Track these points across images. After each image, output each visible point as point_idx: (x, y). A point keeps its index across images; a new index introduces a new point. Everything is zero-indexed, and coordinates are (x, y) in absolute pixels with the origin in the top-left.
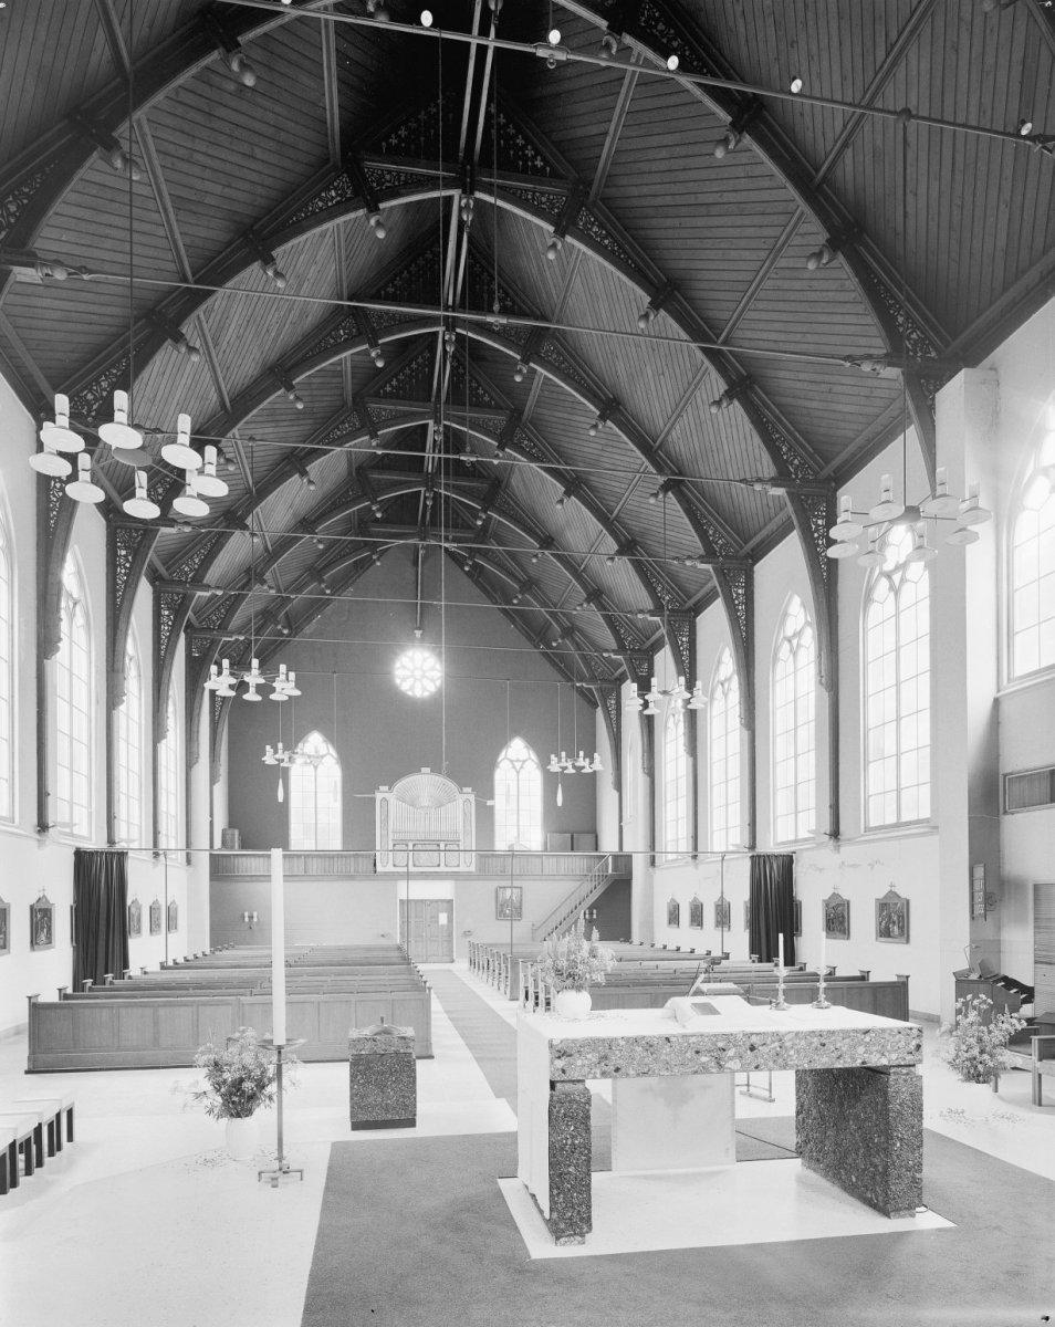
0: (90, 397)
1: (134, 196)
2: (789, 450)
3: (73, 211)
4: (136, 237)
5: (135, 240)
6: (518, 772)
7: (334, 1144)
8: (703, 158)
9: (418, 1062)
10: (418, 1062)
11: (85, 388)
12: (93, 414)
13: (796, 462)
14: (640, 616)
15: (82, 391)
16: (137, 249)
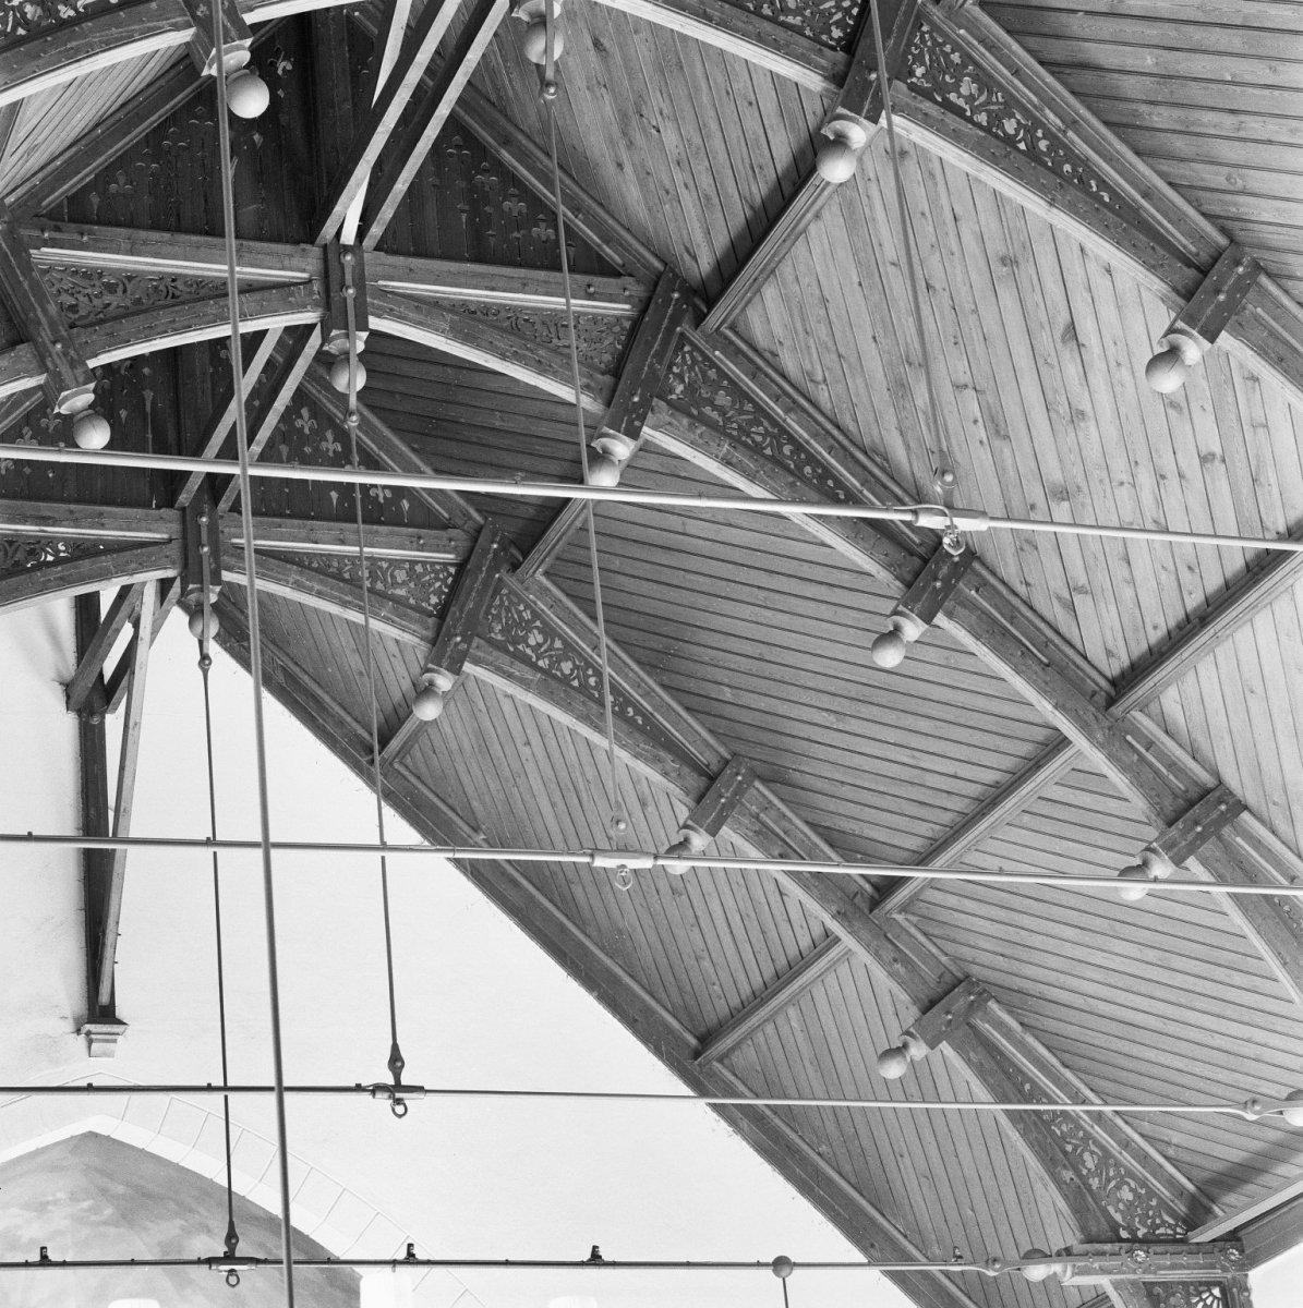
14: (1037, 1272)
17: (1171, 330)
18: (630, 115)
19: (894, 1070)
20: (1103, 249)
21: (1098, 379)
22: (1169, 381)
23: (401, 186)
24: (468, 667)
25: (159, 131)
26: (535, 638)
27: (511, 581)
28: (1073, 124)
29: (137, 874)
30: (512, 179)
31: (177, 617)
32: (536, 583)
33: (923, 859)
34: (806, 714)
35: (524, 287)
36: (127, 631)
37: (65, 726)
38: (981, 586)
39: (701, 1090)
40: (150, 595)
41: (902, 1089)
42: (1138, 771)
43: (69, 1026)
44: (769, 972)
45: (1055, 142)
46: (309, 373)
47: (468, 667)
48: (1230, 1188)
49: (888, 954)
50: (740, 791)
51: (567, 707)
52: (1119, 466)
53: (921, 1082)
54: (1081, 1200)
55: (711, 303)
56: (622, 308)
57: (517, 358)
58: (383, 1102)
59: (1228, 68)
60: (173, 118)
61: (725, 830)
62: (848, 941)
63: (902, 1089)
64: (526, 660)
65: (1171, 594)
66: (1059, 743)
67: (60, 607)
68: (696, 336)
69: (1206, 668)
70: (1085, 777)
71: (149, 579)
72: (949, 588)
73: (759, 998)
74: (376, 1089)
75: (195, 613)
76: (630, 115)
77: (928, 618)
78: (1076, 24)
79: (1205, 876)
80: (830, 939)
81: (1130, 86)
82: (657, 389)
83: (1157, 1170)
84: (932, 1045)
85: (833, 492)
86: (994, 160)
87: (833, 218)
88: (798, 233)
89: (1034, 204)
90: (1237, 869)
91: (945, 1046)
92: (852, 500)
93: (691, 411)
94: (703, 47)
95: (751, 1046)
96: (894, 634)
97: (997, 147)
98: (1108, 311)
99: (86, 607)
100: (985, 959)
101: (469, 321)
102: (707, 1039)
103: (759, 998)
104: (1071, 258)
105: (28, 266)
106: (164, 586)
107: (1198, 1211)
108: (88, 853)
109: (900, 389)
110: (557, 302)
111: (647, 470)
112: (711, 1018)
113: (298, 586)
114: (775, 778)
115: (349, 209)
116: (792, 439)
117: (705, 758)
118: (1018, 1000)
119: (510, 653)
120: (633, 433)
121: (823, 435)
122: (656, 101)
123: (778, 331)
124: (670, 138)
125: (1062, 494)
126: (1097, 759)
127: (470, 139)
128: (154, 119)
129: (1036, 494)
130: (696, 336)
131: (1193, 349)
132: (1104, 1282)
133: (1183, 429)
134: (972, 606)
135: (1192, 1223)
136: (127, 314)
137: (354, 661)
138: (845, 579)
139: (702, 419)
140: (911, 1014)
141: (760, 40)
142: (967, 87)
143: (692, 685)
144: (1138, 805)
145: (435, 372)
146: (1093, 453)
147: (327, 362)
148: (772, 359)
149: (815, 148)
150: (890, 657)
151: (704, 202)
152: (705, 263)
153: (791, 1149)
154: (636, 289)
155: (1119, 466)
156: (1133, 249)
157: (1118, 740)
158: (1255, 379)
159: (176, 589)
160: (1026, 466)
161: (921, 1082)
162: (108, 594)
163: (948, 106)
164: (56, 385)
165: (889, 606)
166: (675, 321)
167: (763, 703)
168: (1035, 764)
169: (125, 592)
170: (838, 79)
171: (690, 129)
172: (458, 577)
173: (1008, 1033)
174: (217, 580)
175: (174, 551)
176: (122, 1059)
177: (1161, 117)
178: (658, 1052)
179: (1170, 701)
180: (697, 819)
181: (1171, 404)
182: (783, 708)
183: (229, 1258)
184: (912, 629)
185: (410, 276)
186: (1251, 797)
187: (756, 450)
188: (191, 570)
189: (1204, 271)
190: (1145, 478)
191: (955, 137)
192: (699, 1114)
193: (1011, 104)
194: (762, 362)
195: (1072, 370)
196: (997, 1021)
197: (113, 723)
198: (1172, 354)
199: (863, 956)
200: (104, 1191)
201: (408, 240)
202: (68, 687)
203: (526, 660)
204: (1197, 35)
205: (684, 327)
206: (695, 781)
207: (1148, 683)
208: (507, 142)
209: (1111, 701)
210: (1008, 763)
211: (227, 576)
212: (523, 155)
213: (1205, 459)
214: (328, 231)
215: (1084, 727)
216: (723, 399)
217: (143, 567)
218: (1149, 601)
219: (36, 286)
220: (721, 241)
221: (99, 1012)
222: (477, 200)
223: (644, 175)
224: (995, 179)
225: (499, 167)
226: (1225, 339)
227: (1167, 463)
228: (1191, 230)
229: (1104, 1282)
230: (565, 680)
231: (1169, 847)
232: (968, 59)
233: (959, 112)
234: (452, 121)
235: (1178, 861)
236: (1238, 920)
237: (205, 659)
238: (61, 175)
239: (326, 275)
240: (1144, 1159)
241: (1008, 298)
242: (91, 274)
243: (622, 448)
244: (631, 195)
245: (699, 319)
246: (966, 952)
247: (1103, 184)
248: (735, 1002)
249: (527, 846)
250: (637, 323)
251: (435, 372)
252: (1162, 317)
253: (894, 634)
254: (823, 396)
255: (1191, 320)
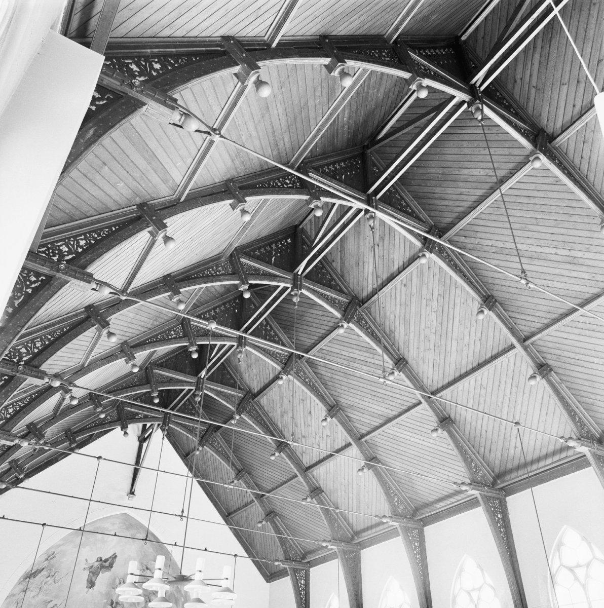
0: (65, 249)
1: (492, 156)
2: (398, 500)
3: (321, 327)
4: (382, 364)
5: (489, 157)
6: (584, 586)
7: (267, 581)
8: (580, 343)
9: (109, 138)
10: (109, 138)
11: (63, 240)
12: (22, 363)
13: (293, 552)
14: (277, 563)
15: (58, 241)
16: (495, 158)
17: (326, 416)
18: (249, 367)
19: (260, 525)
20: (317, 401)
21: (313, 419)
22: (324, 424)
23: (212, 371)
24: (205, 447)
25: (177, 355)
26: (216, 444)
27: (214, 434)
28: (316, 382)
29: (142, 473)
30: (229, 372)
31: (159, 430)
32: (218, 436)
33: (269, 492)
34: (256, 464)
35: (227, 389)
36: (151, 430)
37: (137, 443)
38: (289, 449)
39: (227, 524)
40: (156, 426)
41: (260, 529)
42: (308, 483)
43: (126, 494)
44: (242, 505)
45: (313, 384)
46: (190, 396)
47: (205, 447)
48: (310, 554)
49: (262, 505)
50: (244, 475)
51: (219, 456)
52: (314, 434)
53: (263, 529)
54: (285, 552)
55: (256, 397)
56: (242, 395)
57: (224, 400)
58: (179, 518)
59: (341, 378)
60: (180, 353)
61: (240, 481)
62: (256, 502)
63: (260, 529)
64: (214, 447)
65: (318, 456)
66: (296, 476)
67: (140, 425)
68: (252, 402)
69: (321, 468)
70: (299, 483)
71: (157, 423)
72: (284, 449)
73: (239, 509)
74: (179, 516)
75: (163, 430)
76: (249, 367)
77: (280, 453)
78: (319, 367)
79: (316, 503)
80: (253, 501)
81: (326, 378)
82: (245, 409)
83: (299, 549)
84: (267, 522)
85: (273, 435)
86: (304, 385)
87: (277, 388)
88: (271, 389)
89: (308, 393)
90: (321, 502)
91: (268, 523)
92: (275, 436)
93: (250, 414)
94: (262, 359)
95: (236, 517)
96: (274, 454)
97: (305, 383)
98: (316, 411)
99: (144, 426)
100: (277, 509)
101: (218, 393)
102: (229, 514)
103: (239, 509)
104: (312, 401)
105: (152, 372)
106: (159, 425)
107: (304, 557)
108: (135, 468)
109: (282, 416)
110: (235, 393)
111: (241, 423)
112: (231, 511)
113: (181, 429)
114: (250, 473)
115: (203, 373)
116: (264, 421)
117: (239, 468)
118: (281, 516)
119: (212, 446)
120: (240, 415)
121: (268, 419)
122: (253, 365)
123: (265, 403)
124: (255, 371)
125: (304, 437)
126: (302, 480)
127: (225, 367)
128: (177, 353)
129: (300, 437)
130: (252, 402)
131: (329, 419)
132: (287, 567)
133: (324, 431)
134: (287, 452)
135: (302, 559)
136: (166, 382)
137: (186, 442)
138: (268, 444)
139: (251, 415)
140: (264, 516)
141: (272, 360)
142: (302, 373)
143: (239, 456)
144: (307, 488)
145: (209, 399)
146: (310, 431)
147: (194, 395)
148: (263, 407)
149: (277, 378)
150: (273, 458)
151: (258, 382)
152: (256, 391)
153: (239, 535)
154: (244, 393)
155: (314, 434)
156: (323, 403)
157: (305, 477)
158: (337, 425)
159: (160, 426)
160: (299, 431)
161: (263, 529)
162: (148, 424)
163: (298, 376)
164: (153, 391)
165: (274, 450)
166: (249, 399)
167: (251, 461)
168: (292, 479)
169: (152, 425)
170: (283, 369)
171: (258, 371)
172: (206, 432)
173: (279, 523)
174: (168, 425)
175: (162, 419)
176: (134, 501)
177: (330, 383)
178: (221, 515)
179: (315, 473)
180: (236, 478)
181: (323, 426)
182: (254, 463)
183: (146, 539)
184: (277, 454)
185: (210, 384)
186: (324, 490)
187: (258, 421)
188: (164, 423)
189: (332, 408)
190: (317, 437)
191: (299, 381)
192: (226, 529)
193: (308, 377)
194: (261, 407)
195: (309, 418)
196: (278, 520)
197: (145, 445)
198: (326, 419)
199: (258, 504)
200: (125, 523)
201: (211, 379)
202: (139, 437)
203: (214, 447)
204: (337, 373)
205: (251, 400)
206: (237, 472)
207: (312, 469)
208: (229, 367)
209: (306, 471)
210: (288, 478)
211: (170, 425)
212: (231, 369)
213: (327, 436)
214: (200, 375)
215: (301, 474)
216: (254, 412)
217: (157, 421)
218: (314, 457)
219: (153, 376)
220: (259, 388)
221: (132, 493)
222: (223, 375)
223: (249, 375)
224: (303, 388)
225: (227, 370)
226: (334, 419)
227: (321, 436)
228: (331, 401)
229: (287, 567)
230: (219, 452)
231: (311, 496)
232: (302, 369)
233: (300, 377)
234: (222, 363)
235: (312, 499)
236: (319, 510)
237: (163, 438)
238: (161, 359)
239: (197, 383)
240: (297, 547)
241: (302, 406)
242: (162, 375)
243: (237, 417)
244: (247, 379)
245: (253, 399)
246: (275, 507)
247: (319, 392)
248: (235, 509)
249: (207, 479)
250: (243, 398)
251: (209, 399)
252: (325, 413)
253: (274, 454)
254: (270, 415)
255: (329, 415)
